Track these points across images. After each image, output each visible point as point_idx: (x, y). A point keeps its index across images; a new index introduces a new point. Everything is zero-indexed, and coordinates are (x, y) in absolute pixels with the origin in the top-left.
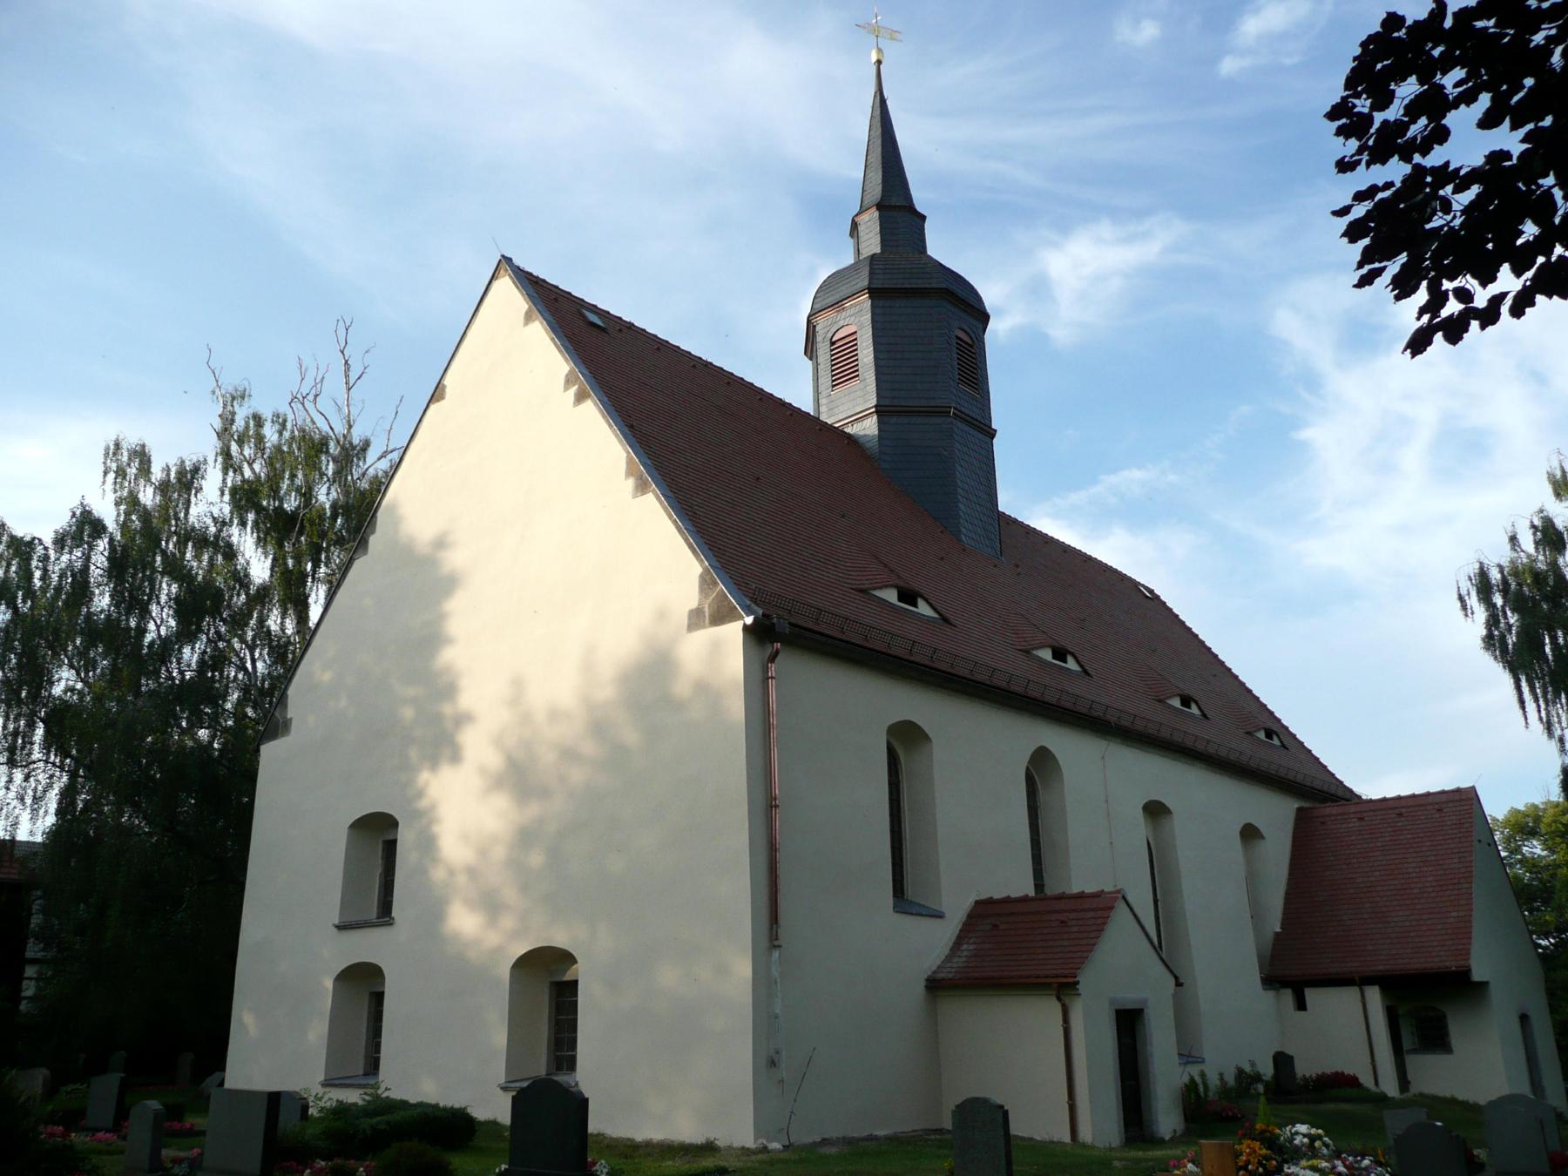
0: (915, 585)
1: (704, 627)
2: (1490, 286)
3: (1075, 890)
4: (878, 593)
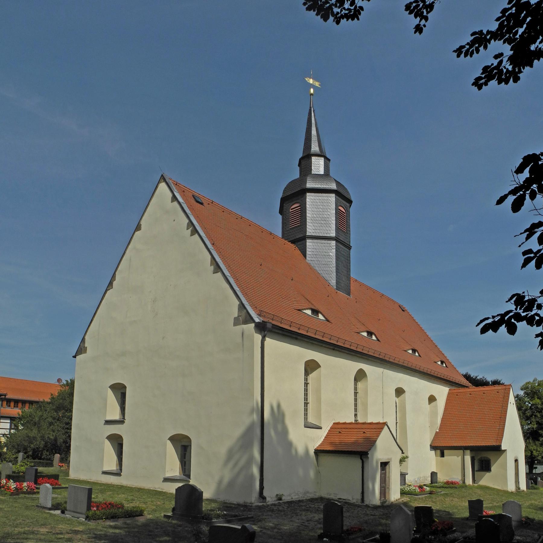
0: (318, 307)
1: (240, 324)
2: (54, 463)
3: (369, 421)
4: (304, 311)
